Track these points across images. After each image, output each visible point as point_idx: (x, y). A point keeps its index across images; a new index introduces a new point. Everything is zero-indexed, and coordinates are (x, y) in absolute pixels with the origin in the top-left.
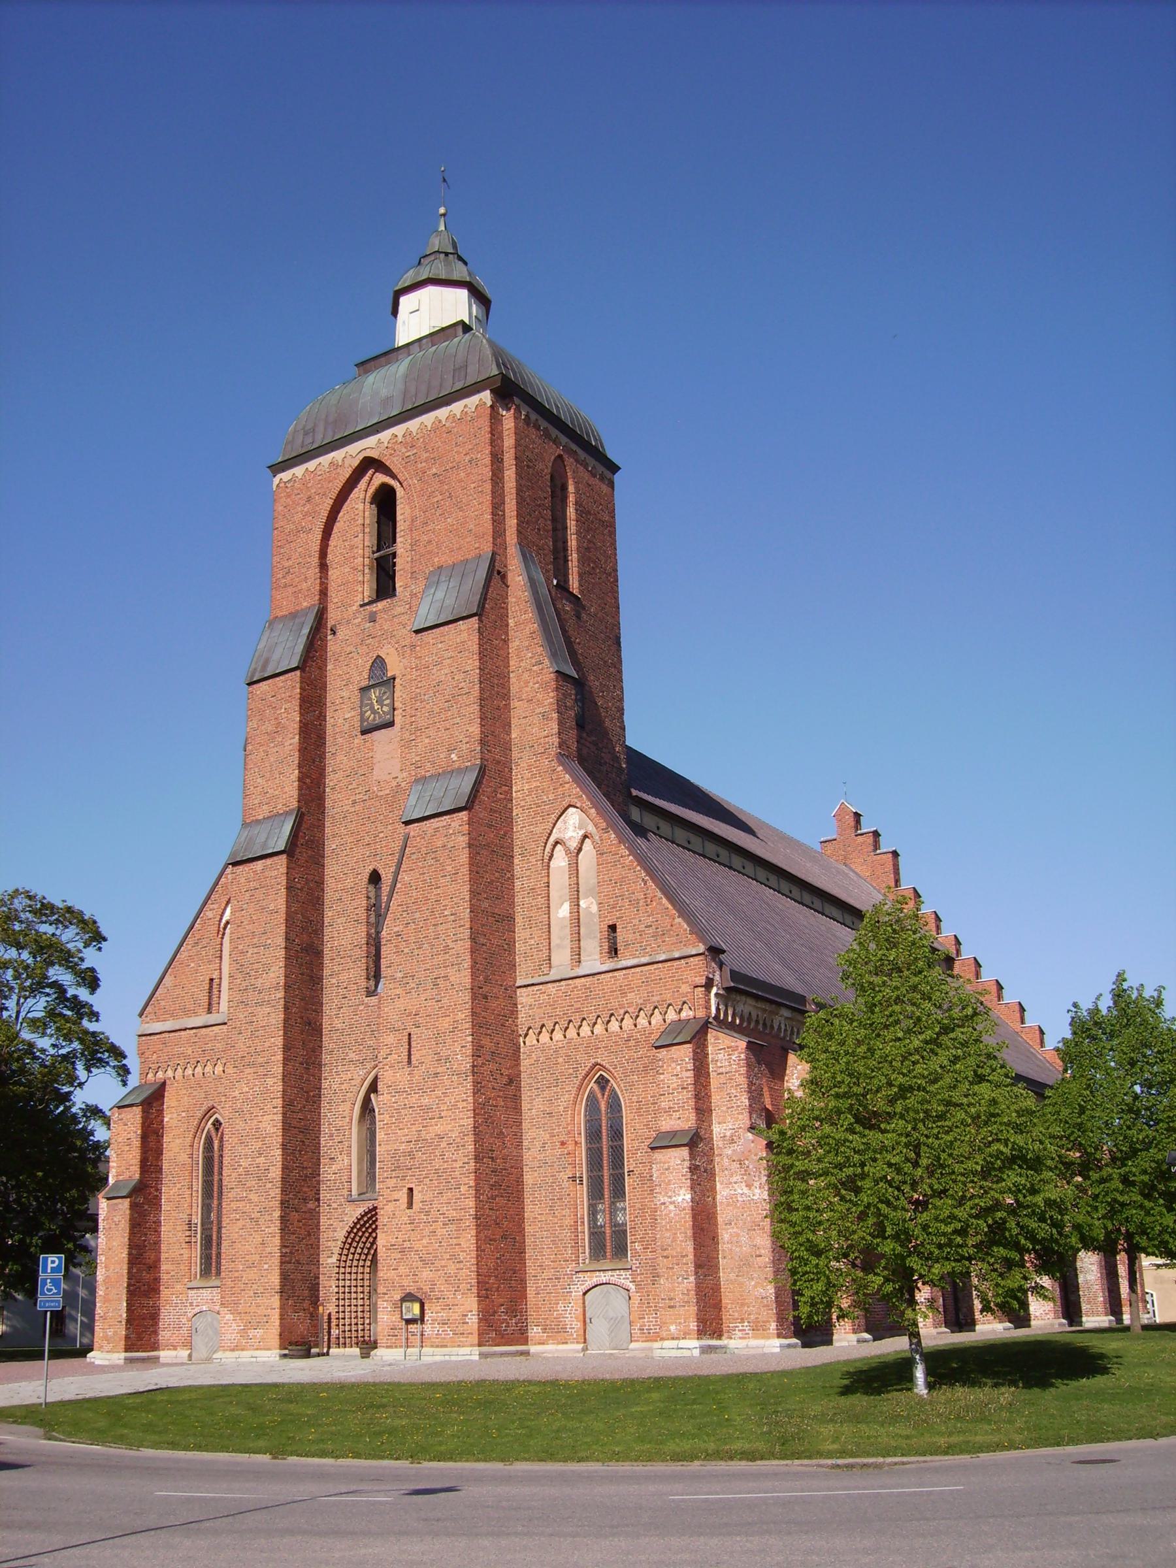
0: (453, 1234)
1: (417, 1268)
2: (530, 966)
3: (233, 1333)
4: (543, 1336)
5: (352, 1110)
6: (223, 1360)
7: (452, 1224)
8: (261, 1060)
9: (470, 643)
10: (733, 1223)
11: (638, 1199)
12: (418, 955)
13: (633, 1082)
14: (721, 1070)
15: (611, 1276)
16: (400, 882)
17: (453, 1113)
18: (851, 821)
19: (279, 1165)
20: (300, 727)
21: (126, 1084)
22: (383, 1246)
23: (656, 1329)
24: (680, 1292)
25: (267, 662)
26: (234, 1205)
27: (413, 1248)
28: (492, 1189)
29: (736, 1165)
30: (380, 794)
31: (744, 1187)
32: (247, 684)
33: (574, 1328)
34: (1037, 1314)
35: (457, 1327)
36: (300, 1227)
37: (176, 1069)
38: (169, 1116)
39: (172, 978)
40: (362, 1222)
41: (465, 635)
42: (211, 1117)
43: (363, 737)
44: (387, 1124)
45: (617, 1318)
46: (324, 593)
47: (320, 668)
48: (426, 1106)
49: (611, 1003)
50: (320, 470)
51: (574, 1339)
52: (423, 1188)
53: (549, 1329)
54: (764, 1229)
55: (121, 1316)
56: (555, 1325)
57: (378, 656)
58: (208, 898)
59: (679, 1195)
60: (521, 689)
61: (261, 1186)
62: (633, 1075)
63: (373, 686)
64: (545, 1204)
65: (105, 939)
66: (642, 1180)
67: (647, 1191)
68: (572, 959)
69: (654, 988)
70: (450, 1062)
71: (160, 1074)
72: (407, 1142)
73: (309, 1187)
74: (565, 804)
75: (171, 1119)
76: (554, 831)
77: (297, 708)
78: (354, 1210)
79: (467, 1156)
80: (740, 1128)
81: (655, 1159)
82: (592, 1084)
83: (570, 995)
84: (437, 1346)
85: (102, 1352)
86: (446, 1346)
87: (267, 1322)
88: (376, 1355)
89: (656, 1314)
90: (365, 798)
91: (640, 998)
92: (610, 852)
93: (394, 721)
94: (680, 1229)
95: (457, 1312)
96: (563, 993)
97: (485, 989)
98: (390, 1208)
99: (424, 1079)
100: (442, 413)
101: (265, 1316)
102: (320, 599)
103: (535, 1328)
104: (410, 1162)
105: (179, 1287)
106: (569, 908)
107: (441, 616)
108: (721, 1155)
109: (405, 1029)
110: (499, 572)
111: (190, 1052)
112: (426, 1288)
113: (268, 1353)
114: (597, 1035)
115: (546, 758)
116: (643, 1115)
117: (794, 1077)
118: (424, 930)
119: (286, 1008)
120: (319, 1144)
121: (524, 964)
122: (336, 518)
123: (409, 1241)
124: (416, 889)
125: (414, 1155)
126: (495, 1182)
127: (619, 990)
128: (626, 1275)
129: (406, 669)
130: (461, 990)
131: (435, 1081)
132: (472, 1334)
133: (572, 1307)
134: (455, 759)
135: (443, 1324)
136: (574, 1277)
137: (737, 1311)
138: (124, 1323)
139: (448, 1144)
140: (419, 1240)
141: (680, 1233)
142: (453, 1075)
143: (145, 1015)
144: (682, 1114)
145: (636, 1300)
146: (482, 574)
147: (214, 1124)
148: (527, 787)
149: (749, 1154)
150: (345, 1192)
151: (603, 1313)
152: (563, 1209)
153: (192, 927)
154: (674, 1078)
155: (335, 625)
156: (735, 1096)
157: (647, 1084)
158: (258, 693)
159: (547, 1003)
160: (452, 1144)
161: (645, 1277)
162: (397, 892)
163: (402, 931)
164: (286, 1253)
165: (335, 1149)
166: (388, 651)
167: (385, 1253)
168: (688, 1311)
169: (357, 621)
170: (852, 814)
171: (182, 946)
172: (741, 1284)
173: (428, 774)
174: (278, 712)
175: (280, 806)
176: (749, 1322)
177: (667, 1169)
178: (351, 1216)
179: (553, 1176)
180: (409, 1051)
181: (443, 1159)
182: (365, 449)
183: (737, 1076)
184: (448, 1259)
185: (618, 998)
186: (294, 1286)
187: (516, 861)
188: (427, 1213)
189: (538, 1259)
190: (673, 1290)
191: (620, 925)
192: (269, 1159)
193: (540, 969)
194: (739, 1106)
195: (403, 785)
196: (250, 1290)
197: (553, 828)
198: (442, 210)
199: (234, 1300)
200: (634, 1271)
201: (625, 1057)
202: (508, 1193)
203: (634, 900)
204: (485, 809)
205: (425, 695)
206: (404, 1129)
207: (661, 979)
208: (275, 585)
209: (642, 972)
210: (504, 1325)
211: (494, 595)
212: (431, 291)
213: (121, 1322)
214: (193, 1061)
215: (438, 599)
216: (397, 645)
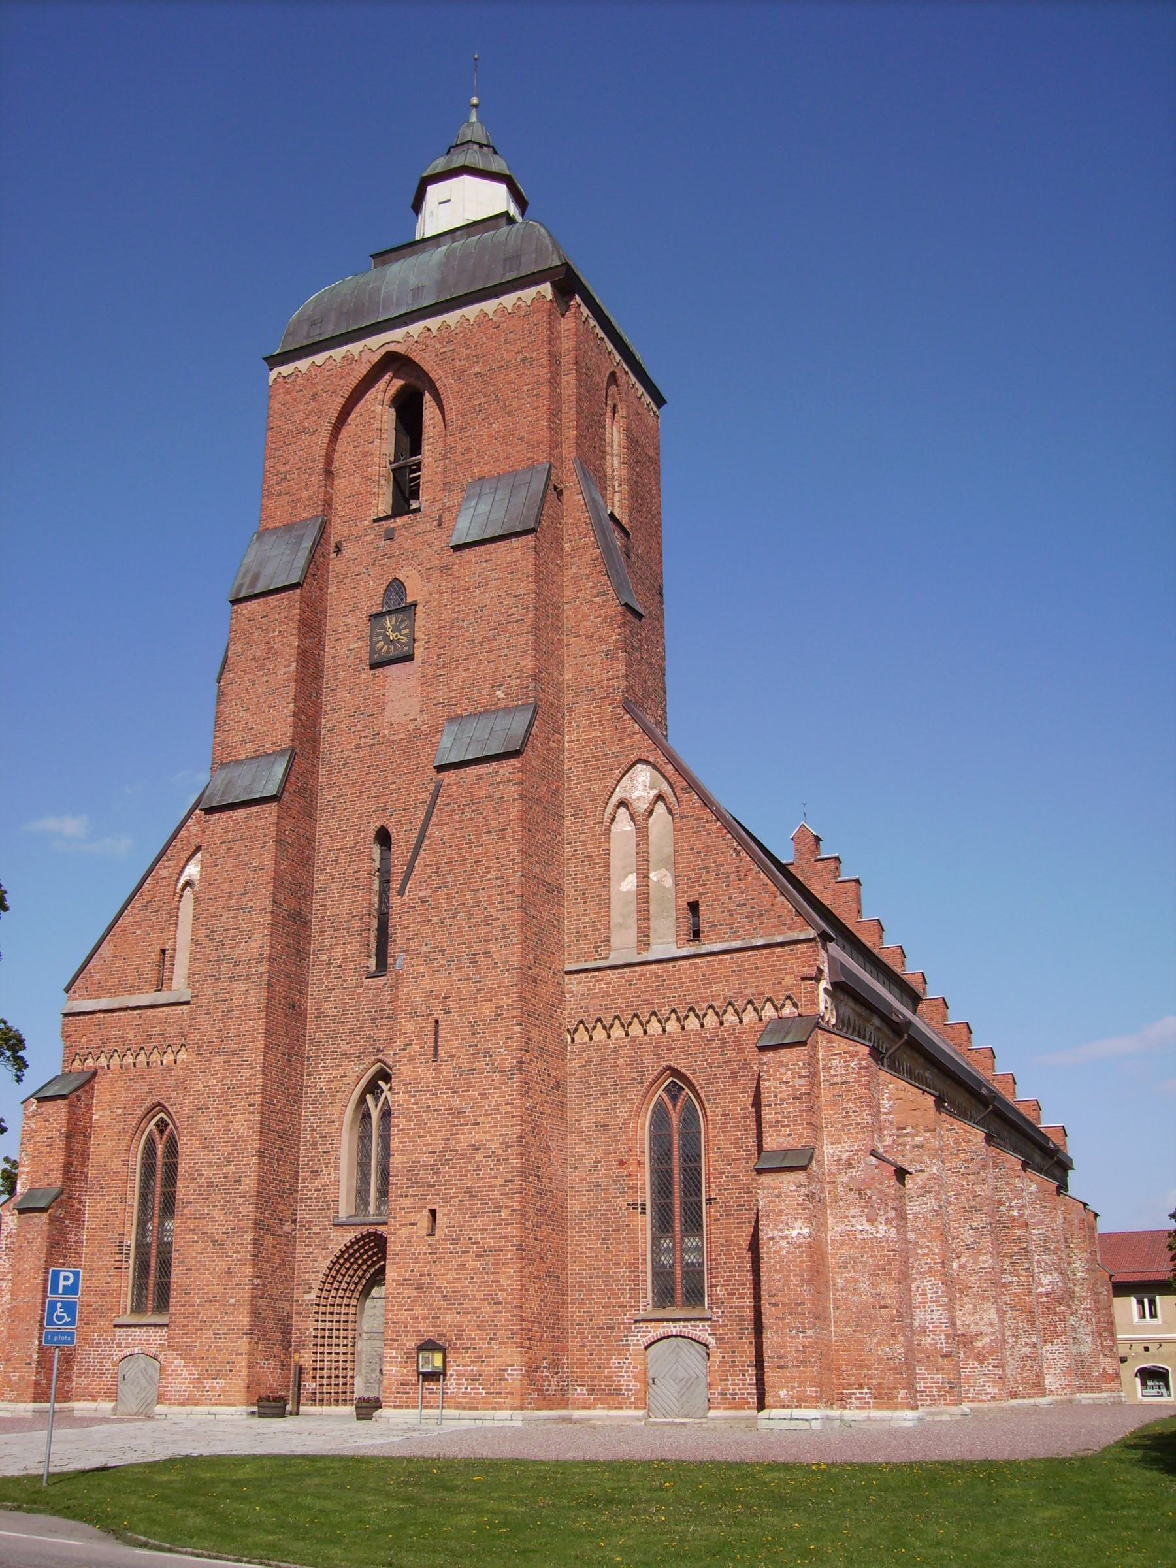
0: (489, 1269)
1: (440, 1309)
2: (584, 948)
3: (184, 1383)
6: (169, 1417)
7: (488, 1256)
8: (233, 1046)
9: (524, 563)
10: (849, 1266)
11: (721, 1233)
12: (451, 925)
13: (717, 1091)
14: (835, 1080)
15: (684, 1327)
16: (428, 838)
17: (492, 1118)
18: (810, 843)
19: (254, 1176)
21: (21, 1081)
22: (393, 1281)
23: (742, 1394)
24: (794, 1349)
27: (435, 1284)
28: (537, 1214)
29: (854, 1195)
30: (395, 738)
31: (864, 1222)
32: (231, 602)
33: (631, 1390)
34: (1053, 1388)
36: (275, 1255)
37: (112, 1056)
38: (100, 1113)
41: (517, 554)
42: (155, 1116)
43: (372, 672)
45: (689, 1379)
46: (328, 503)
47: (321, 589)
51: (631, 1403)
52: (450, 1211)
55: (30, 1356)
56: (606, 1386)
57: (396, 579)
59: (793, 1228)
61: (229, 1201)
62: (717, 1082)
64: (595, 1235)
67: (734, 1223)
68: (639, 941)
71: (90, 1062)
72: (429, 1153)
74: (633, 758)
75: (101, 1116)
76: (618, 789)
77: (295, 632)
78: (343, 1236)
79: (510, 1172)
80: (861, 1150)
81: (762, 1184)
82: (660, 1092)
83: (636, 984)
84: (464, 1408)
86: (476, 1408)
87: (231, 1371)
88: (380, 1417)
89: (744, 1375)
90: (372, 742)
91: (729, 990)
92: (691, 816)
93: (413, 654)
94: (794, 1270)
96: (626, 981)
97: (535, 970)
98: (404, 1233)
100: (490, 306)
101: (228, 1363)
102: (323, 511)
103: (578, 1388)
104: (432, 1178)
105: (103, 1323)
106: (635, 880)
107: (488, 531)
108: (834, 1182)
109: (430, 1015)
110: (555, 488)
111: (131, 1036)
112: (452, 1335)
113: (232, 1409)
114: (670, 1033)
115: (610, 704)
118: (460, 897)
120: (298, 1153)
121: (575, 945)
122: (346, 420)
124: (450, 847)
125: (439, 1169)
126: (541, 1206)
127: (701, 980)
128: (703, 1326)
129: (431, 594)
130: (507, 970)
131: (470, 1079)
132: (512, 1394)
133: (630, 1363)
134: (502, 696)
136: (633, 1326)
137: (853, 1375)
142: (495, 1072)
143: (72, 990)
144: (793, 1130)
146: (538, 485)
147: (157, 1125)
148: (583, 736)
149: (872, 1181)
150: (331, 1213)
152: (619, 1243)
153: (140, 886)
154: (783, 1085)
155: (340, 542)
156: (854, 1112)
158: (245, 612)
159: (604, 992)
160: (490, 1157)
161: (729, 1330)
162: (425, 850)
164: (258, 1285)
165: (319, 1160)
166: (409, 574)
167: (395, 1289)
168: (804, 1372)
169: (368, 538)
170: (813, 838)
171: (126, 909)
172: (859, 1341)
173: (465, 714)
174: (270, 635)
175: (269, 745)
176: (868, 1389)
177: (777, 1196)
178: (338, 1243)
180: (436, 1041)
181: (477, 1175)
183: (857, 1087)
184: (481, 1299)
186: (265, 1327)
187: (567, 823)
189: (585, 1304)
190: (784, 1346)
191: (703, 902)
192: (241, 1169)
193: (597, 951)
194: (859, 1124)
195: (423, 728)
198: (475, 101)
199: (186, 1342)
200: (715, 1321)
201: (707, 1060)
203: (723, 873)
207: (757, 968)
210: (546, 1384)
211: (550, 512)
212: (466, 179)
213: (30, 1364)
215: (481, 512)
216: (420, 568)
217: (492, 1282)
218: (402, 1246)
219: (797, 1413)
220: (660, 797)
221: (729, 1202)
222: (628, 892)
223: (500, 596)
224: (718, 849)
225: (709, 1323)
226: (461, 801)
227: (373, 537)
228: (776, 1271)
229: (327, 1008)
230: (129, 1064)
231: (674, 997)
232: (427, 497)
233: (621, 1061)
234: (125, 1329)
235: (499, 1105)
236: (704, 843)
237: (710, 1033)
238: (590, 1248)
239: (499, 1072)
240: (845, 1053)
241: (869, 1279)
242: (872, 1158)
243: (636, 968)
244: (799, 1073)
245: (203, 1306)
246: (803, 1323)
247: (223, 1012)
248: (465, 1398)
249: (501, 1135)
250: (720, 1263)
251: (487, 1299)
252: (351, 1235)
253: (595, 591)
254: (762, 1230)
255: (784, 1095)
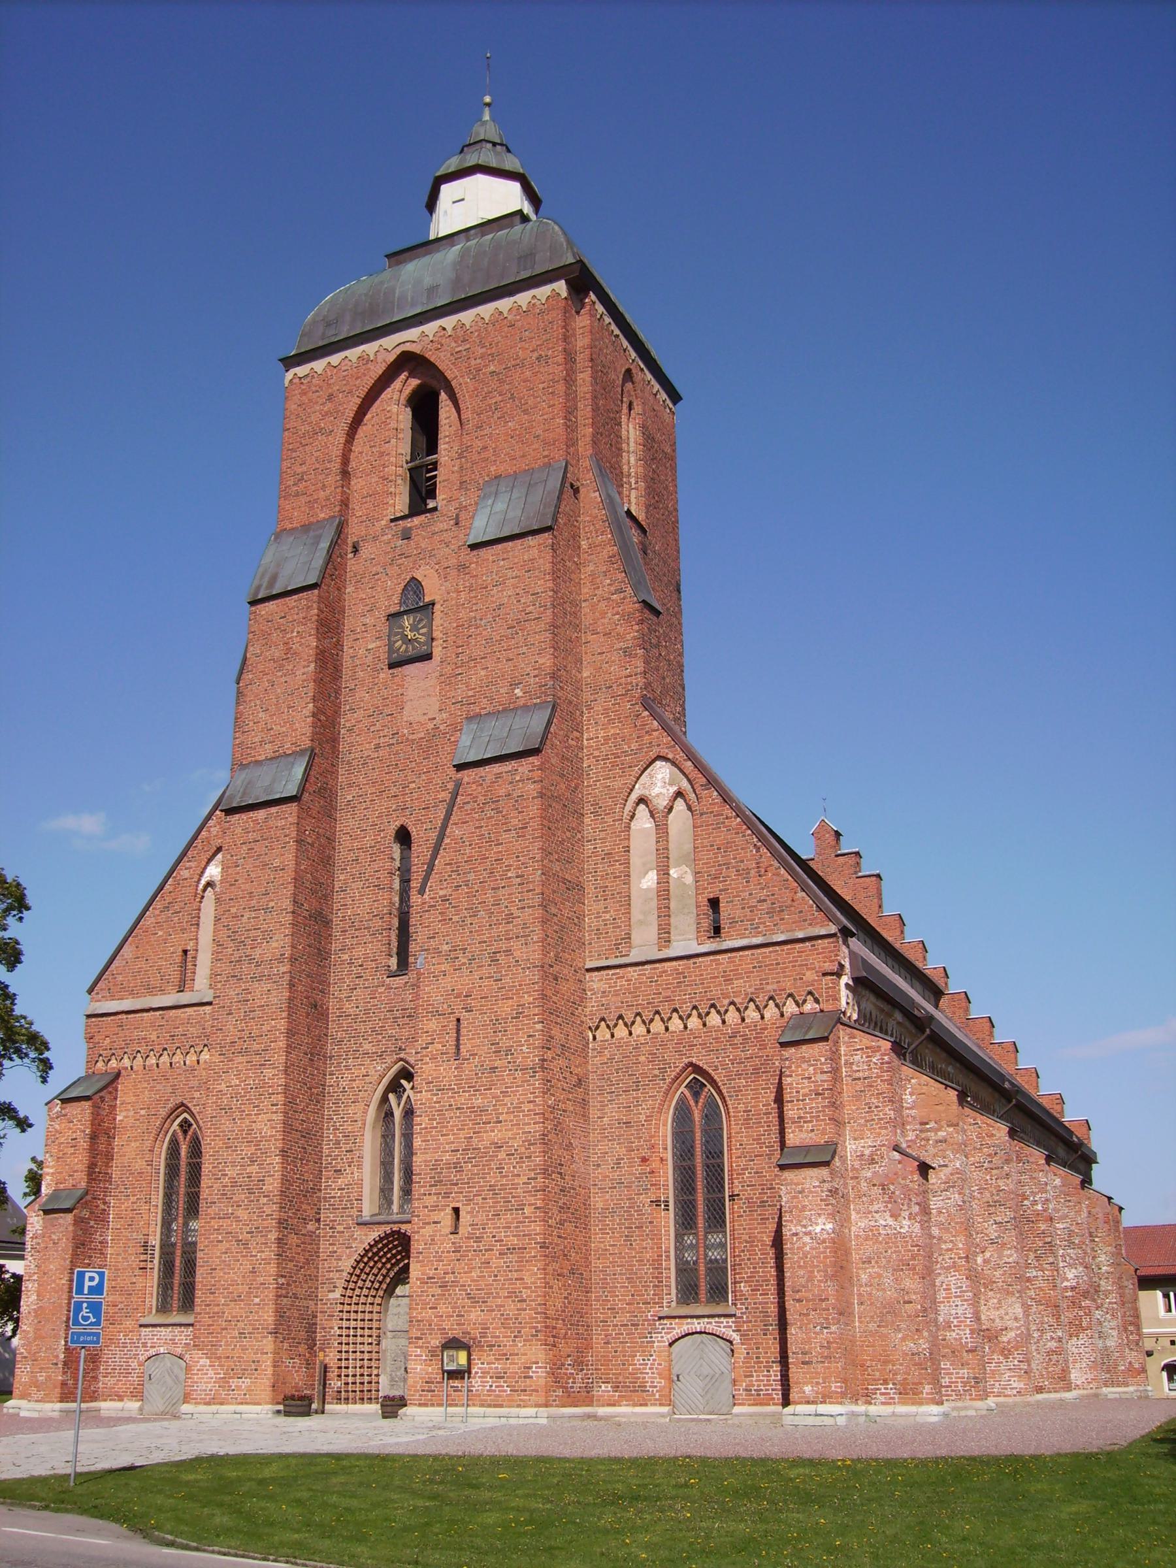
1: (464, 1307)
2: (604, 946)
3: (210, 1383)
4: (614, 1396)
5: (365, 1112)
6: (195, 1416)
7: (512, 1253)
8: (256, 1047)
9: (541, 561)
11: (744, 1229)
12: (471, 924)
13: (739, 1087)
14: (857, 1075)
15: (708, 1323)
17: (515, 1116)
18: (830, 838)
19: (278, 1175)
20: (317, 654)
22: (417, 1279)
23: (767, 1390)
25: (274, 579)
26: (215, 1224)
27: (459, 1282)
28: (560, 1212)
29: (877, 1191)
30: (414, 737)
33: (656, 1387)
34: (1079, 1383)
35: (517, 1382)
36: (299, 1254)
37: (135, 1057)
38: (124, 1114)
39: (133, 948)
40: (375, 1250)
42: (178, 1117)
43: (391, 671)
44: (426, 1128)
46: (345, 503)
47: (339, 589)
48: (479, 1107)
49: (711, 991)
50: (346, 365)
51: (656, 1400)
53: (622, 1387)
54: (915, 1269)
56: (630, 1383)
57: (413, 579)
58: (184, 854)
59: (817, 1224)
60: (595, 622)
62: (739, 1079)
63: (406, 612)
64: (618, 1233)
65: (28, 908)
66: (750, 1207)
67: (757, 1219)
68: (659, 938)
69: (769, 974)
70: (513, 1054)
71: (113, 1063)
72: (452, 1151)
73: (309, 1204)
74: (652, 755)
75: (126, 1117)
76: (637, 786)
78: (366, 1235)
79: (533, 1170)
80: (884, 1145)
81: (784, 1180)
82: (682, 1089)
83: (656, 981)
84: (489, 1406)
85: (29, 1401)
86: (501, 1406)
87: (256, 1370)
91: (750, 987)
93: (432, 653)
94: (818, 1266)
95: (517, 1364)
96: (647, 978)
98: (427, 1231)
99: (476, 1074)
100: (504, 304)
101: (254, 1362)
103: (603, 1385)
105: (129, 1323)
106: (656, 877)
108: (857, 1178)
109: (451, 1013)
110: (572, 486)
111: (154, 1037)
113: (258, 1408)
114: (691, 1030)
115: (628, 701)
116: (752, 1127)
117: (907, 1092)
118: (480, 895)
119: (292, 985)
121: (596, 943)
122: (362, 420)
123: (453, 1273)
124: (470, 845)
125: (461, 1167)
128: (728, 1322)
129: (448, 593)
130: (529, 968)
133: (654, 1360)
134: (520, 694)
135: (497, 1377)
136: (657, 1323)
137: (878, 1370)
138: (60, 1366)
139: (507, 1155)
140: (465, 1273)
141: (818, 1271)
143: (95, 992)
144: (816, 1126)
145: (741, 1351)
146: (554, 482)
147: (181, 1126)
148: (602, 734)
150: (354, 1212)
151: (695, 1369)
152: (643, 1240)
153: (161, 888)
156: (876, 1107)
157: (758, 1089)
159: (625, 989)
160: (513, 1155)
161: (754, 1326)
162: (445, 849)
163: (451, 895)
164: (283, 1284)
167: (420, 1287)
168: (829, 1368)
169: (385, 537)
171: (148, 910)
173: (483, 712)
174: (289, 636)
176: (894, 1384)
177: (800, 1192)
178: (362, 1242)
179: (630, 1199)
180: (458, 1040)
181: (500, 1173)
182: (404, 343)
184: (505, 1297)
185: (721, 985)
187: (587, 821)
188: (479, 1240)
189: (609, 1301)
191: (724, 899)
192: (265, 1168)
194: (882, 1119)
195: (442, 727)
196: (234, 1329)
197: (636, 783)
198: (487, 99)
199: (212, 1341)
201: (729, 1056)
202: (576, 1218)
203: (743, 870)
204: (557, 755)
205: (481, 619)
206: (448, 1135)
207: (778, 964)
208: (283, 493)
209: (753, 954)
212: (480, 178)
213: (56, 1364)
214: (158, 1048)
216: (437, 567)
217: (516, 1279)
218: (425, 1244)
219: (822, 1408)
220: (679, 794)
221: (752, 1198)
222: (648, 890)
223: (518, 594)
224: (738, 845)
225: (734, 1319)
226: (481, 799)
227: (390, 536)
228: (800, 1267)
229: (349, 1008)
230: (152, 1065)
231: (695, 993)
232: (444, 496)
233: (642, 1059)
234: (150, 1329)
235: (521, 1103)
236: (724, 839)
237: (732, 1029)
238: (614, 1245)
239: (521, 1070)
240: (867, 1048)
241: (893, 1275)
242: (895, 1153)
243: (657, 965)
244: (821, 1069)
245: (228, 1305)
246: (827, 1319)
247: (245, 1012)
248: (489, 1396)
249: (523, 1133)
250: (744, 1260)
251: (511, 1297)
252: (374, 1234)
253: (612, 589)
254: (786, 1226)
255: (806, 1090)
